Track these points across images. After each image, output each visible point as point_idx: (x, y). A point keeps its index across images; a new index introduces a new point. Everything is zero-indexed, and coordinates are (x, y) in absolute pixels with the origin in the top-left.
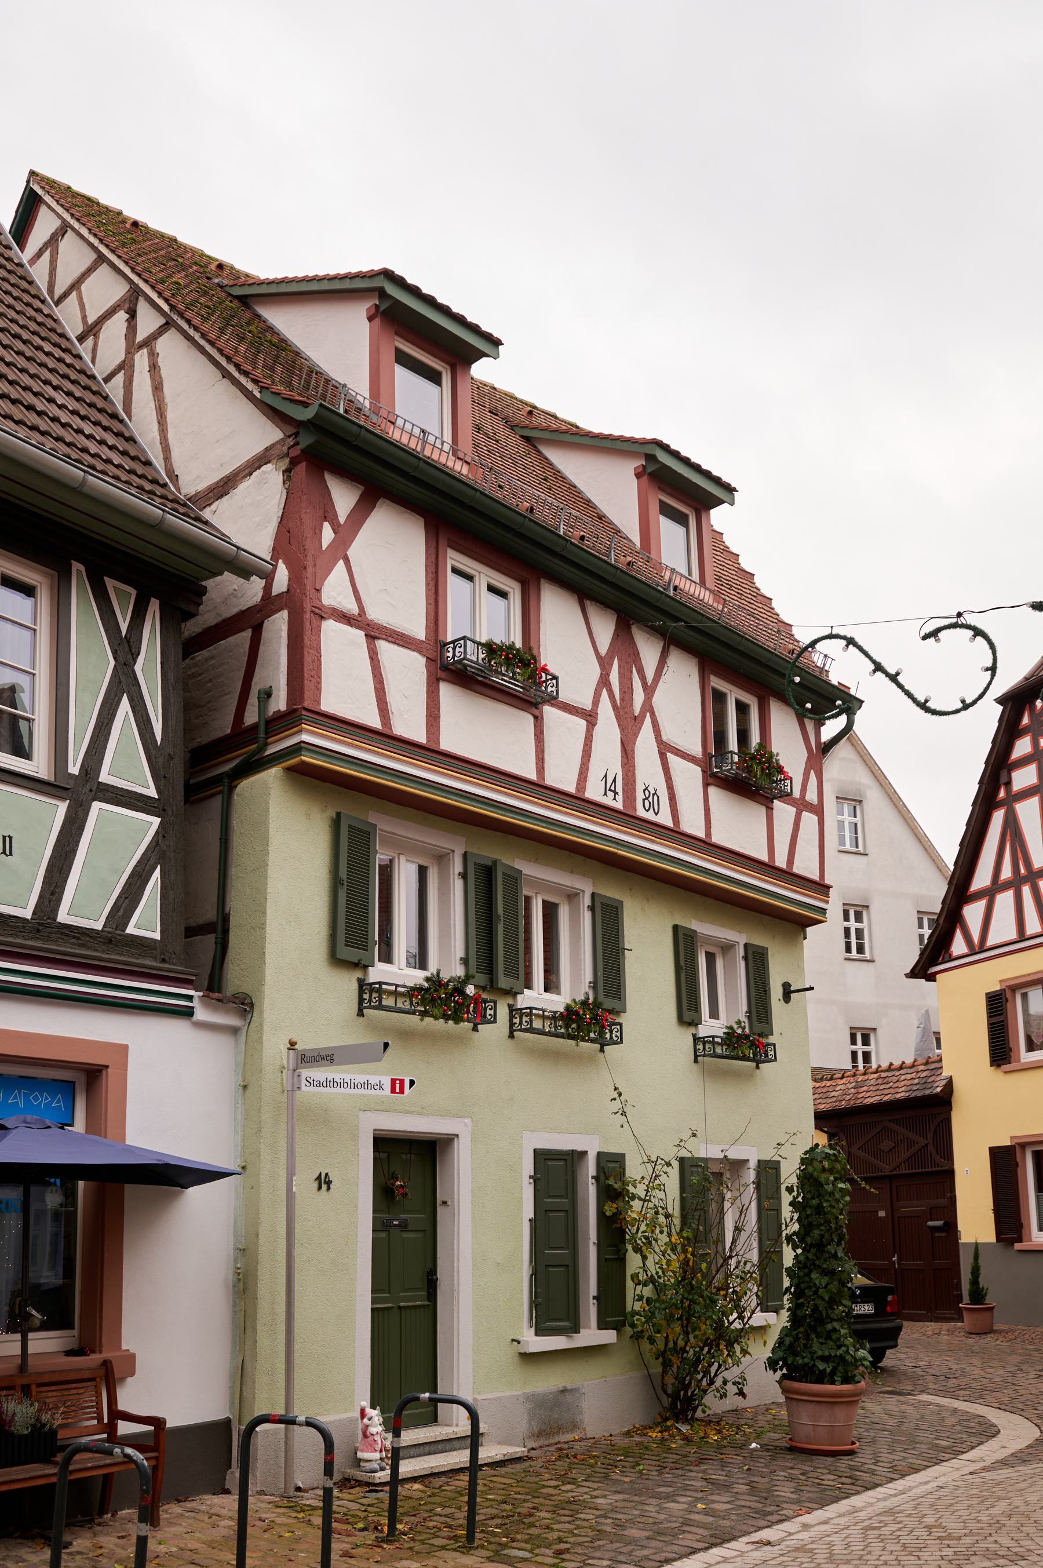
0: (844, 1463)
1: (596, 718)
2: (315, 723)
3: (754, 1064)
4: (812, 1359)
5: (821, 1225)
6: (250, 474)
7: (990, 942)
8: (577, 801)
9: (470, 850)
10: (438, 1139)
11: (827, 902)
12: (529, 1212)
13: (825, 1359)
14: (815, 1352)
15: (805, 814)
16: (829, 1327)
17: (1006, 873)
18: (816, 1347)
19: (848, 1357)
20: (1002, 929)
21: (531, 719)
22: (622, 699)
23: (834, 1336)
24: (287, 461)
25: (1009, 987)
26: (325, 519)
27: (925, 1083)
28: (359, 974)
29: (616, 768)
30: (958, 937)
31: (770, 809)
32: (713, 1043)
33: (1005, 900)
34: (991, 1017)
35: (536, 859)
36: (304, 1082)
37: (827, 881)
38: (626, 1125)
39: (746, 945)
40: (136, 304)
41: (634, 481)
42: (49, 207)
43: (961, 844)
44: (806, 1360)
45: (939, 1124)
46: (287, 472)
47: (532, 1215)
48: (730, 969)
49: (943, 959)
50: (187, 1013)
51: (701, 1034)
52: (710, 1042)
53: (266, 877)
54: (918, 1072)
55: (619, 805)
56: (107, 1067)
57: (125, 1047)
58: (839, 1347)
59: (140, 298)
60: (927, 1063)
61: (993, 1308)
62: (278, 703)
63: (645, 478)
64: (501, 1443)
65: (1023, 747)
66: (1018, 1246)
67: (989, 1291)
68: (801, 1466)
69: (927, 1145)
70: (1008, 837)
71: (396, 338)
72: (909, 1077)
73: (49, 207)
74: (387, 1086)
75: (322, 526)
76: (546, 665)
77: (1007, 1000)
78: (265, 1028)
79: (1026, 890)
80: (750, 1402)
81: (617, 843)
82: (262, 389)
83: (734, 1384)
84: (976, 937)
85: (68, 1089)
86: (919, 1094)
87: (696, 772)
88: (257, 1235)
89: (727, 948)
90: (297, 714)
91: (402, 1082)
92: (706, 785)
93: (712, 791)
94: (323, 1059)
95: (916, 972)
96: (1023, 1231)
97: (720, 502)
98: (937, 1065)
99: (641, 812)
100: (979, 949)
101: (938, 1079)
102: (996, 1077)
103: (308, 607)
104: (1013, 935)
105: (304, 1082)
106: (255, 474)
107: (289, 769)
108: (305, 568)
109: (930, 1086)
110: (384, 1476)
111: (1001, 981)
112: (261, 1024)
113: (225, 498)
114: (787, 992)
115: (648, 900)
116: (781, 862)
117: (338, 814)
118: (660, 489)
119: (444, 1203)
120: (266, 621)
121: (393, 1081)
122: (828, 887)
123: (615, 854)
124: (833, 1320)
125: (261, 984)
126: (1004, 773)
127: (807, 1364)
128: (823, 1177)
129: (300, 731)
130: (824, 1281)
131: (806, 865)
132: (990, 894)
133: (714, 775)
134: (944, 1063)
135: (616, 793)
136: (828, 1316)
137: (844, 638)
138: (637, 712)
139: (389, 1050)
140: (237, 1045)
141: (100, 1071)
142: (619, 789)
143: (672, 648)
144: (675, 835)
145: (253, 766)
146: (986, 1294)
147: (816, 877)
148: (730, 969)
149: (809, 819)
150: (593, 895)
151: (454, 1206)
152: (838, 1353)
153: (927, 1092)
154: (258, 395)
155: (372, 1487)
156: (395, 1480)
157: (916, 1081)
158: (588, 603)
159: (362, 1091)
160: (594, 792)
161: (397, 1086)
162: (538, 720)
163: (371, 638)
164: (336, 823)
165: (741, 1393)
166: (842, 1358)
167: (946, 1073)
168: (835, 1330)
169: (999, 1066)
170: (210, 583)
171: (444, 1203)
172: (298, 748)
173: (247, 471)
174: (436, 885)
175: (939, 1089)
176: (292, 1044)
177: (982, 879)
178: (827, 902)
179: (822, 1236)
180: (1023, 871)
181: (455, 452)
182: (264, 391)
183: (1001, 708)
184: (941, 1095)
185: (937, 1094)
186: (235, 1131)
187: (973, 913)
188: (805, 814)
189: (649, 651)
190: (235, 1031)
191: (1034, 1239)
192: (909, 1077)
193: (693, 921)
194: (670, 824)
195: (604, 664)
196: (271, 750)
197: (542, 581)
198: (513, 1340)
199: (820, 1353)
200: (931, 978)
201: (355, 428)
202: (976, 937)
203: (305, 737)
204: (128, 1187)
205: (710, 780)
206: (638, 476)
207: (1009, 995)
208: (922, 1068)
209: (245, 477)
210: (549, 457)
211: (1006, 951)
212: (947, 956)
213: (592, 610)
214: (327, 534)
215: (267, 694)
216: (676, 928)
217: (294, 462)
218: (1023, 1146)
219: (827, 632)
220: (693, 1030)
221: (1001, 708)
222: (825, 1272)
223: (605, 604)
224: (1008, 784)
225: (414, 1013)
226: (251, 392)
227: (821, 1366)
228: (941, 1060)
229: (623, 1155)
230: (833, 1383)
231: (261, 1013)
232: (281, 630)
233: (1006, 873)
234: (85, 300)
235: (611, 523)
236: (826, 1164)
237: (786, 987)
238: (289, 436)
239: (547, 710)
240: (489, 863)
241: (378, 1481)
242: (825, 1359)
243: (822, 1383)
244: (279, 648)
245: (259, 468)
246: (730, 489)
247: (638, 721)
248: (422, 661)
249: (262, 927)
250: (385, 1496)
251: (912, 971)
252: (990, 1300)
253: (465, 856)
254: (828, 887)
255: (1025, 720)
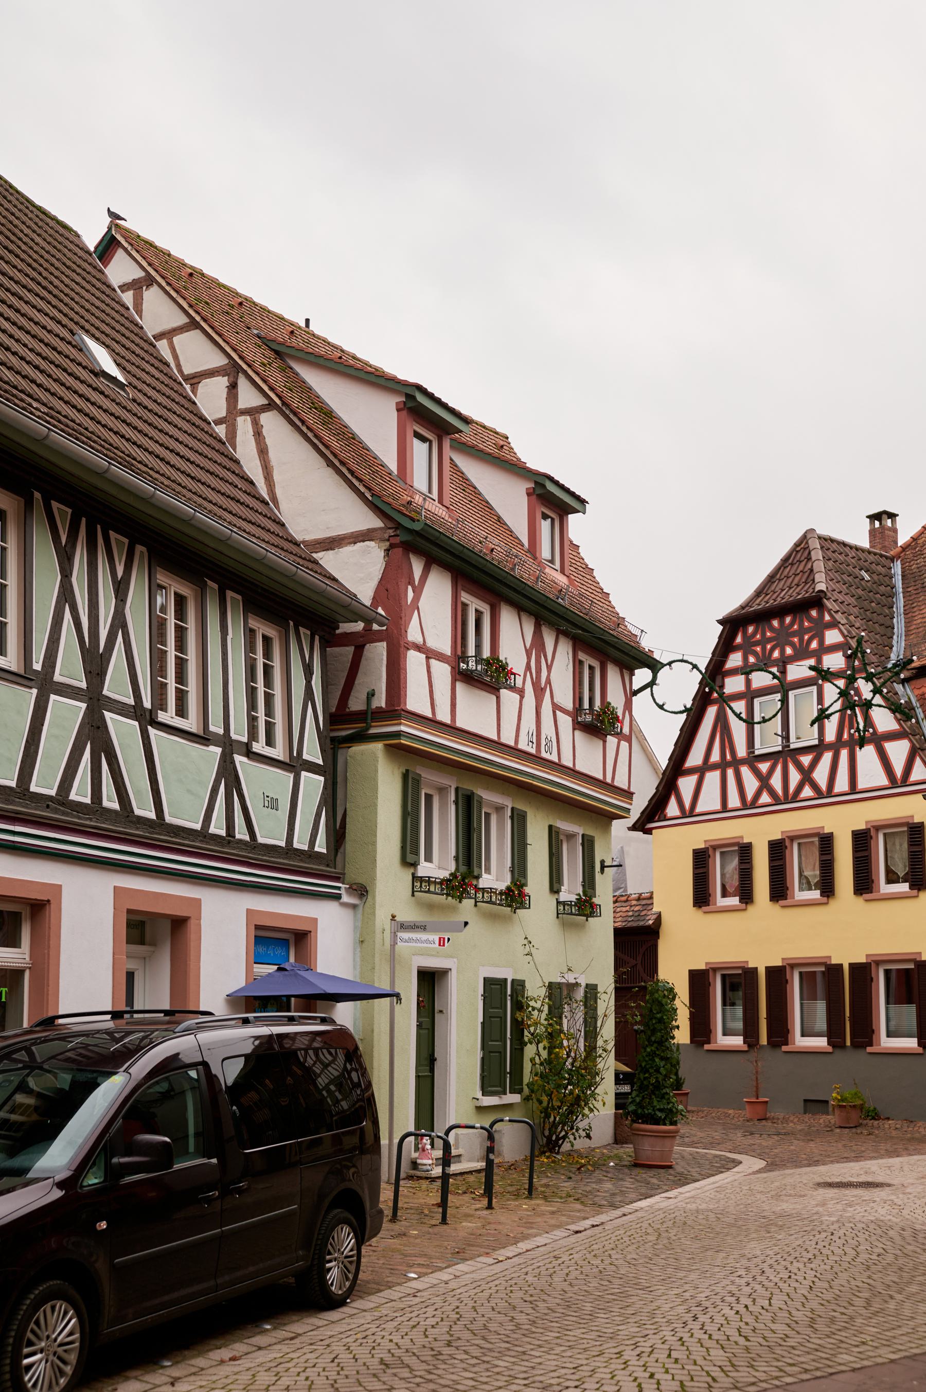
0: (671, 1171)
1: (524, 693)
2: (406, 719)
3: (585, 918)
4: (654, 1110)
5: (662, 1029)
6: (355, 543)
7: (699, 809)
8: (514, 751)
9: (460, 786)
10: (437, 971)
11: (631, 804)
12: (481, 1020)
13: (661, 1110)
14: (656, 1106)
15: (622, 742)
16: (664, 1091)
17: (715, 757)
18: (655, 1103)
19: (674, 1110)
20: (709, 800)
21: (495, 698)
22: (536, 678)
23: (667, 1097)
24: (388, 544)
25: (711, 846)
26: (409, 584)
27: (638, 915)
28: (412, 870)
29: (533, 727)
30: (673, 802)
31: (605, 742)
32: (571, 905)
33: (712, 779)
34: (696, 868)
35: (487, 788)
36: (399, 940)
37: (632, 790)
38: (532, 962)
39: (583, 835)
40: (237, 379)
41: (525, 499)
42: (126, 250)
43: (681, 730)
44: (650, 1111)
45: (647, 949)
46: (387, 551)
47: (482, 1020)
48: (572, 851)
49: (659, 818)
50: (337, 897)
51: (561, 900)
52: (568, 905)
53: (376, 813)
54: (631, 906)
55: (533, 751)
56: (310, 932)
57: (316, 920)
58: (668, 1103)
59: (240, 374)
60: (639, 899)
61: (688, 1093)
62: (380, 701)
63: (534, 497)
64: (469, 1161)
65: (735, 660)
66: (707, 1047)
67: (686, 1081)
68: (644, 1174)
69: (636, 965)
70: (719, 729)
71: (414, 423)
72: (624, 909)
73: (126, 250)
74: (437, 942)
75: (407, 588)
76: (512, 668)
77: (709, 856)
78: (377, 907)
79: (730, 772)
80: (593, 1143)
81: (533, 777)
82: (373, 495)
83: (584, 1130)
84: (687, 804)
85: (285, 943)
86: (635, 924)
87: (569, 720)
88: (373, 1031)
89: (570, 837)
90: (397, 713)
91: (444, 939)
92: (574, 729)
93: (577, 733)
94: (418, 927)
95: (637, 826)
96: (874, 1036)
97: (576, 511)
98: (649, 902)
99: (544, 755)
100: (689, 813)
101: (649, 913)
102: (697, 916)
103: (402, 643)
104: (718, 806)
105: (399, 940)
106: (359, 544)
107: (386, 745)
108: (401, 618)
109: (642, 918)
110: (437, 1171)
111: (705, 841)
112: (374, 904)
113: (331, 552)
114: (603, 867)
115: (538, 809)
116: (609, 780)
117: (407, 771)
118: (542, 504)
119: (441, 1011)
120: (368, 645)
121: (440, 939)
122: (632, 794)
123: (532, 784)
124: (666, 1087)
125: (373, 879)
126: (719, 678)
127: (650, 1114)
128: (664, 1001)
129: (400, 724)
130: (662, 1064)
131: (621, 782)
132: (701, 771)
133: (579, 723)
134: (655, 900)
135: (533, 743)
136: (663, 1085)
137: (691, 663)
138: (543, 685)
139: (468, 927)
140: (355, 916)
141: (307, 934)
142: (534, 741)
143: (560, 636)
144: (557, 767)
145: (362, 737)
146: (683, 1083)
147: (625, 787)
148: (572, 851)
149: (624, 745)
150: (513, 809)
151: (447, 1013)
152: (669, 1107)
153: (641, 923)
154: (370, 498)
155: (433, 1180)
156: (445, 1177)
157: (631, 914)
158: (522, 613)
159: (425, 945)
160: (523, 745)
161: (442, 942)
162: (498, 698)
163: (428, 658)
164: (405, 777)
165: (588, 1136)
166: (671, 1110)
167: (656, 909)
168: (667, 1093)
169: (700, 907)
170: (341, 624)
171: (441, 1011)
172: (398, 735)
173: (351, 540)
174: (438, 807)
175: (651, 922)
176: (393, 917)
177: (695, 758)
178: (631, 804)
179: (663, 1036)
180: (728, 757)
181: (441, 501)
182: (374, 497)
183: (721, 628)
184: (652, 927)
185: (649, 927)
186: (355, 968)
187: (686, 785)
188: (622, 742)
189: (549, 640)
190: (354, 907)
191: (719, 1042)
192: (624, 909)
193: (558, 821)
194: (556, 760)
195: (528, 653)
196: (373, 731)
197: (502, 604)
198: (474, 1098)
199: (658, 1107)
200: (648, 832)
201: (437, 534)
202: (687, 804)
203: (403, 728)
204: (318, 1002)
205: (577, 726)
206: (529, 494)
207: (711, 852)
208: (634, 902)
209: (350, 543)
210: (464, 470)
211: (710, 817)
212: (662, 816)
213: (524, 617)
214: (410, 594)
215: (371, 695)
216: (550, 827)
217: (392, 546)
218: (715, 970)
219: (681, 658)
220: (556, 896)
221: (721, 628)
222: (662, 1059)
223: (530, 613)
224: (722, 686)
225: (443, 895)
226: (363, 494)
227: (659, 1114)
228: (651, 898)
229: (524, 981)
230: (665, 1124)
231: (374, 897)
232: (383, 655)
233: (715, 757)
234: (178, 351)
235: (505, 524)
236: (666, 993)
237: (602, 862)
238: (389, 528)
239: (504, 692)
240: (469, 793)
241: (433, 1176)
242: (661, 1110)
243: (659, 1125)
244: (381, 666)
245: (363, 541)
246: (583, 502)
247: (543, 690)
248: (449, 668)
249: (374, 844)
250: (439, 1183)
251: (634, 825)
252: (686, 1089)
253: (457, 789)
254: (632, 794)
255: (739, 639)
